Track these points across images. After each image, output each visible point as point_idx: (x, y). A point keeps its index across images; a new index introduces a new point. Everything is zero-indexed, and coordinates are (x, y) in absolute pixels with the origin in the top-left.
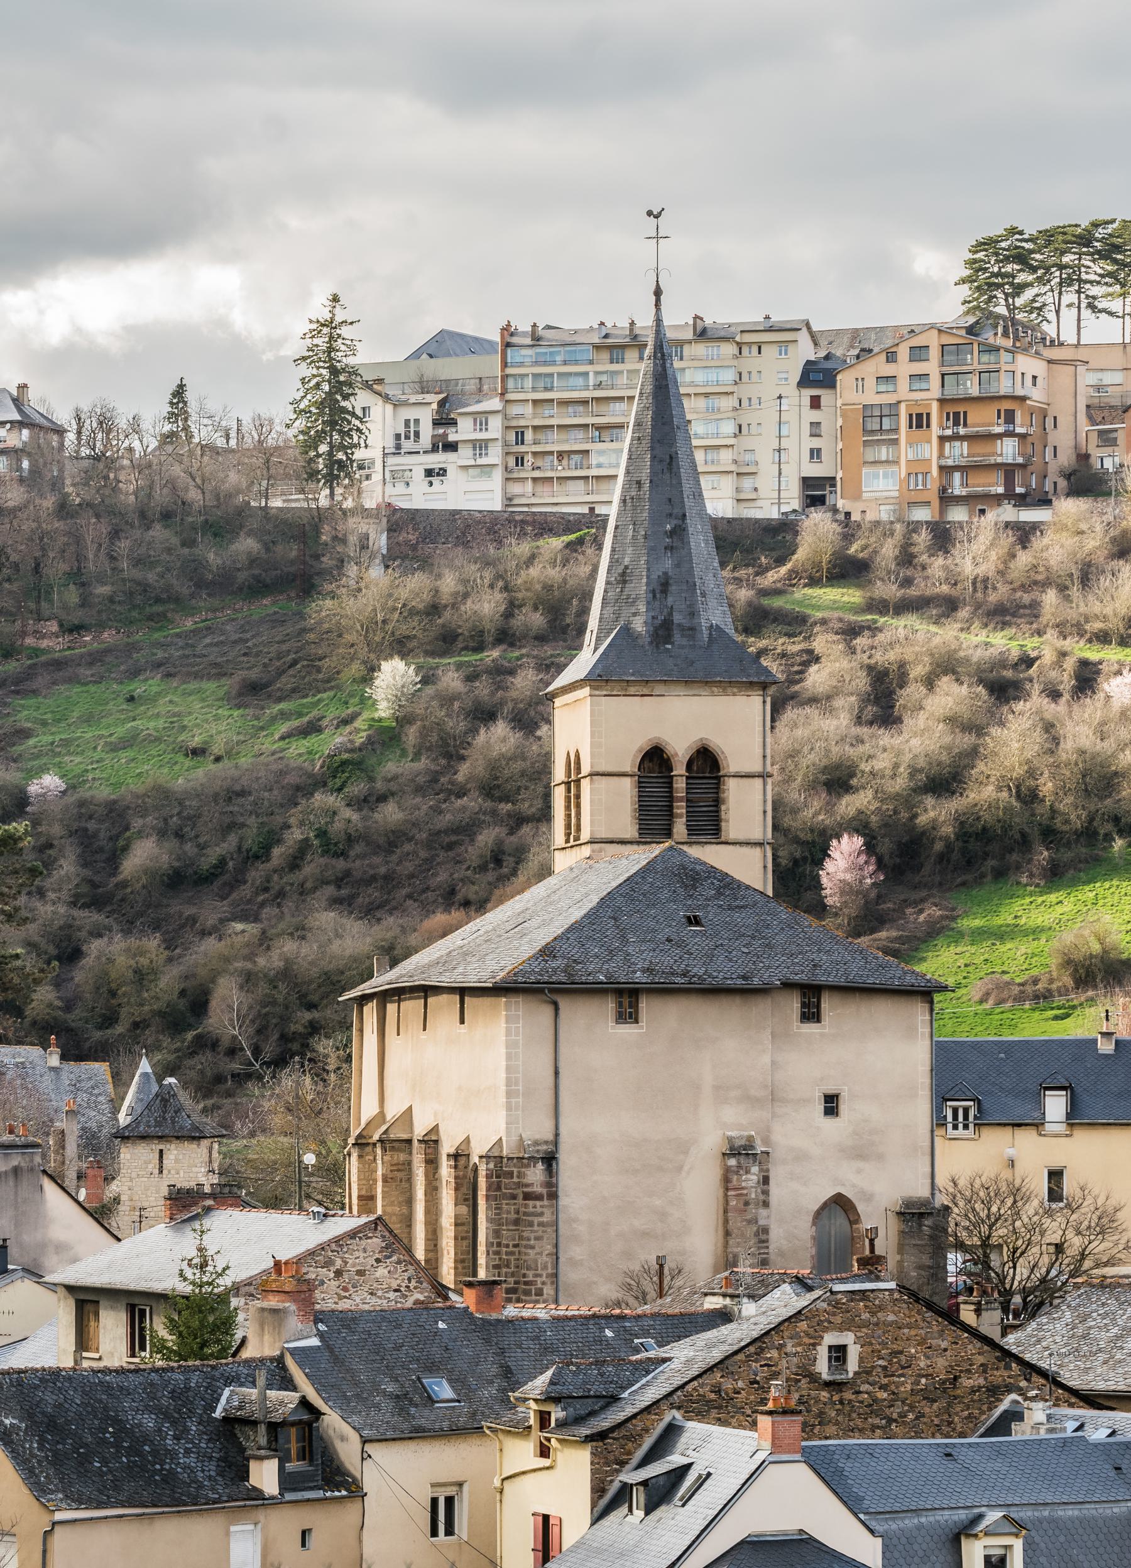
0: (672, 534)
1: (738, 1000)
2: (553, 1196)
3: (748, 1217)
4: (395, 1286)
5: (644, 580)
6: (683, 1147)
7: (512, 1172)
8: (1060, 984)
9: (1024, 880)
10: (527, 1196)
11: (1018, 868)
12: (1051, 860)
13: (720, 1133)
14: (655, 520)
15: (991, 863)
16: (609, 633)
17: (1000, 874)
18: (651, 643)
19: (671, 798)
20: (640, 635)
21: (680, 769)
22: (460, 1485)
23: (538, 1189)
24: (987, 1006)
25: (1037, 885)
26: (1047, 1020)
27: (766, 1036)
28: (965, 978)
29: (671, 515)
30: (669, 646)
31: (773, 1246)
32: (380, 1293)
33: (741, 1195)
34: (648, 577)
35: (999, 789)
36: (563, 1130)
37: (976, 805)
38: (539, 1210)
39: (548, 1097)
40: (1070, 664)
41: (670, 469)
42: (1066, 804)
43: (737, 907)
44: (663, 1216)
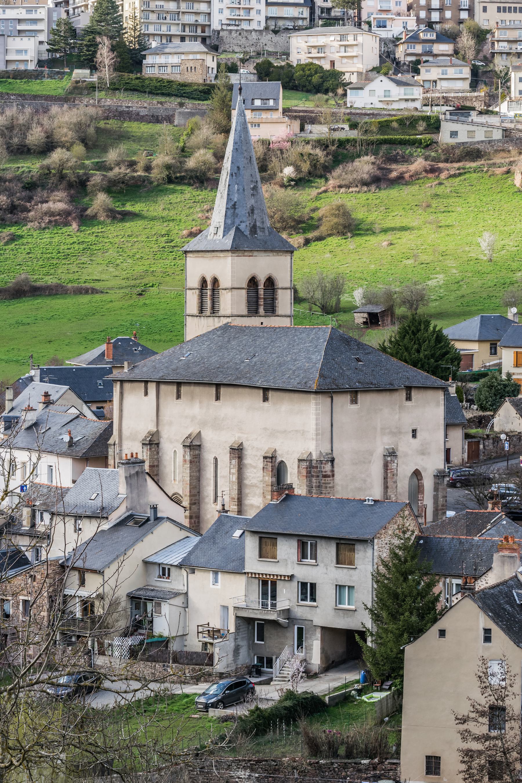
1: (388, 393)
2: (333, 476)
10: (325, 476)
19: (258, 298)
21: (261, 286)
23: (329, 473)
41: (250, 162)
44: (365, 481)
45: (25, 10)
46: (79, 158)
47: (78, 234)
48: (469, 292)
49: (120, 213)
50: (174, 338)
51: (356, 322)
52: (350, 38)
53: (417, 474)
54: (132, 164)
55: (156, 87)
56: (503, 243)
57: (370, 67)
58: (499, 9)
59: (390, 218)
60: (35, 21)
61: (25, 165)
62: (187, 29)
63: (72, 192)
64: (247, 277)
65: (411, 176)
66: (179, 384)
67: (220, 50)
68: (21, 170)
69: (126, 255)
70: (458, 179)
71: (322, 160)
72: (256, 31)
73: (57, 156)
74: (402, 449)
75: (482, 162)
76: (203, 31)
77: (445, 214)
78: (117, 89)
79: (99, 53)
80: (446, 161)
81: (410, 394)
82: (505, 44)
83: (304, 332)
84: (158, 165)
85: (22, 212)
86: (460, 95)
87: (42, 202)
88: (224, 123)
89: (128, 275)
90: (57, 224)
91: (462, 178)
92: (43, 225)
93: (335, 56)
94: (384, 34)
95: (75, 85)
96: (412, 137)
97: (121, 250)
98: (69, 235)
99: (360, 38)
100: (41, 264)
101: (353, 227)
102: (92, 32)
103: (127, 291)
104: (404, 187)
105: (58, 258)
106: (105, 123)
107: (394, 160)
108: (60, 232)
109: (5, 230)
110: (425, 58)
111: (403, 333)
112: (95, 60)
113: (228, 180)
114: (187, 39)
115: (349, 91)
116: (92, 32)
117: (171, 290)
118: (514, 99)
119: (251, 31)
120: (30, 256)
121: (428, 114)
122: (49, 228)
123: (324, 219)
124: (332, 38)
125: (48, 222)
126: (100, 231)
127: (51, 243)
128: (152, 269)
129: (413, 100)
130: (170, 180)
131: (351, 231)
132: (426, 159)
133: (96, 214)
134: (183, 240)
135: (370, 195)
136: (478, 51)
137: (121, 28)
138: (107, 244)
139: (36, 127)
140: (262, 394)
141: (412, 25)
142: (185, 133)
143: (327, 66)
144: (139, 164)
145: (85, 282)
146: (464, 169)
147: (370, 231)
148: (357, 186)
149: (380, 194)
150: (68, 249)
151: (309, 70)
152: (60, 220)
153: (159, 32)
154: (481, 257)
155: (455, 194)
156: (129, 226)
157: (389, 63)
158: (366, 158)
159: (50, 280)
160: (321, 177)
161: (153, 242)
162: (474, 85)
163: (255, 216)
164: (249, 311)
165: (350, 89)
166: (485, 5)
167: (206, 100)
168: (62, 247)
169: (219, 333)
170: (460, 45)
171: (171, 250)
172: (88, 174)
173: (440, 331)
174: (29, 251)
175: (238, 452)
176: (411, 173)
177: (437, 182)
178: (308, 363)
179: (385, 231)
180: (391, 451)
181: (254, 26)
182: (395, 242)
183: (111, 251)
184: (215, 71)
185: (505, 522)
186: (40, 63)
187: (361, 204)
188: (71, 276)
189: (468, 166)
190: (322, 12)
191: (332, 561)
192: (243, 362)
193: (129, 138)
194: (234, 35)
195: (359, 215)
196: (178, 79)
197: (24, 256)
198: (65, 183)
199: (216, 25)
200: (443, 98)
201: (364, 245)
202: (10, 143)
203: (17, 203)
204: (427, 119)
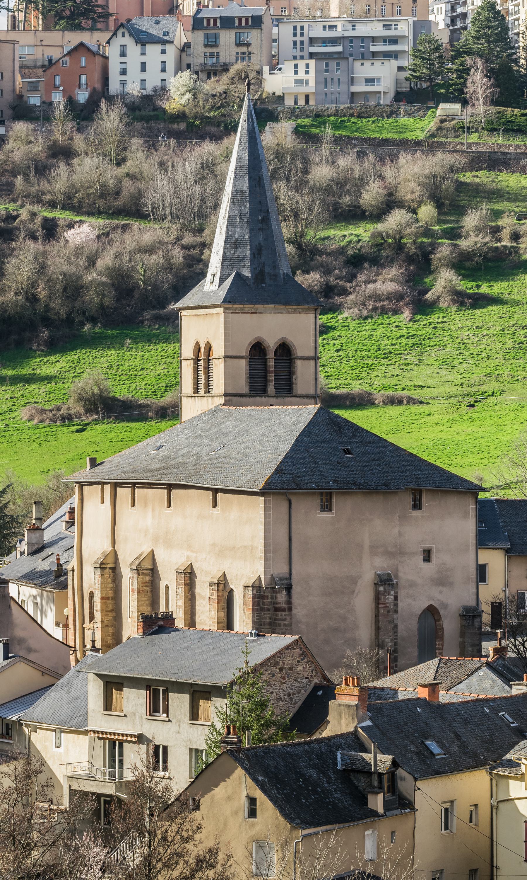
0: (263, 220)
2: (290, 609)
3: (390, 619)
4: (306, 675)
5: (248, 247)
6: (354, 580)
7: (268, 596)
8: (75, 411)
9: (35, 348)
11: (30, 341)
12: (50, 337)
13: (373, 572)
14: (252, 212)
15: (13, 337)
16: (229, 275)
17: (19, 344)
18: (254, 283)
19: (266, 371)
21: (271, 355)
22: (452, 802)
23: (283, 606)
24: (35, 422)
25: (42, 351)
26: (73, 432)
27: (396, 517)
28: (13, 405)
29: (261, 210)
30: (264, 285)
31: (399, 635)
32: (299, 680)
33: (386, 607)
34: (250, 246)
35: (16, 294)
36: (294, 572)
37: (3, 303)
38: (284, 617)
39: (286, 552)
40: (38, 220)
42: (56, 303)
43: (366, 443)
44: (344, 619)
45: (381, 24)
47: (410, 325)
49: (470, 296)
53: (432, 612)
60: (394, 40)
64: (248, 342)
68: (347, 239)
69: (467, 354)
73: (396, 219)
78: (495, 130)
81: (420, 500)
85: (340, 295)
89: (463, 380)
90: (384, 311)
92: (365, 313)
95: (439, 124)
97: (464, 346)
98: (397, 326)
100: (351, 364)
106: (474, 176)
112: (466, 90)
113: (228, 208)
117: (514, 400)
120: (340, 353)
122: (372, 318)
125: (372, 309)
126: (439, 321)
127: (370, 337)
128: (497, 372)
133: (438, 298)
138: (446, 338)
144: (504, 230)
145: (404, 389)
152: (384, 307)
156: (480, 314)
159: (357, 387)
161: (508, 336)
163: (263, 259)
164: (252, 388)
168: (384, 343)
172: (435, 243)
174: (339, 347)
175: (189, 577)
180: (384, 578)
183: (448, 348)
191: (185, 715)
193: (502, 196)
197: (332, 353)
198: (403, 256)
202: (339, 203)
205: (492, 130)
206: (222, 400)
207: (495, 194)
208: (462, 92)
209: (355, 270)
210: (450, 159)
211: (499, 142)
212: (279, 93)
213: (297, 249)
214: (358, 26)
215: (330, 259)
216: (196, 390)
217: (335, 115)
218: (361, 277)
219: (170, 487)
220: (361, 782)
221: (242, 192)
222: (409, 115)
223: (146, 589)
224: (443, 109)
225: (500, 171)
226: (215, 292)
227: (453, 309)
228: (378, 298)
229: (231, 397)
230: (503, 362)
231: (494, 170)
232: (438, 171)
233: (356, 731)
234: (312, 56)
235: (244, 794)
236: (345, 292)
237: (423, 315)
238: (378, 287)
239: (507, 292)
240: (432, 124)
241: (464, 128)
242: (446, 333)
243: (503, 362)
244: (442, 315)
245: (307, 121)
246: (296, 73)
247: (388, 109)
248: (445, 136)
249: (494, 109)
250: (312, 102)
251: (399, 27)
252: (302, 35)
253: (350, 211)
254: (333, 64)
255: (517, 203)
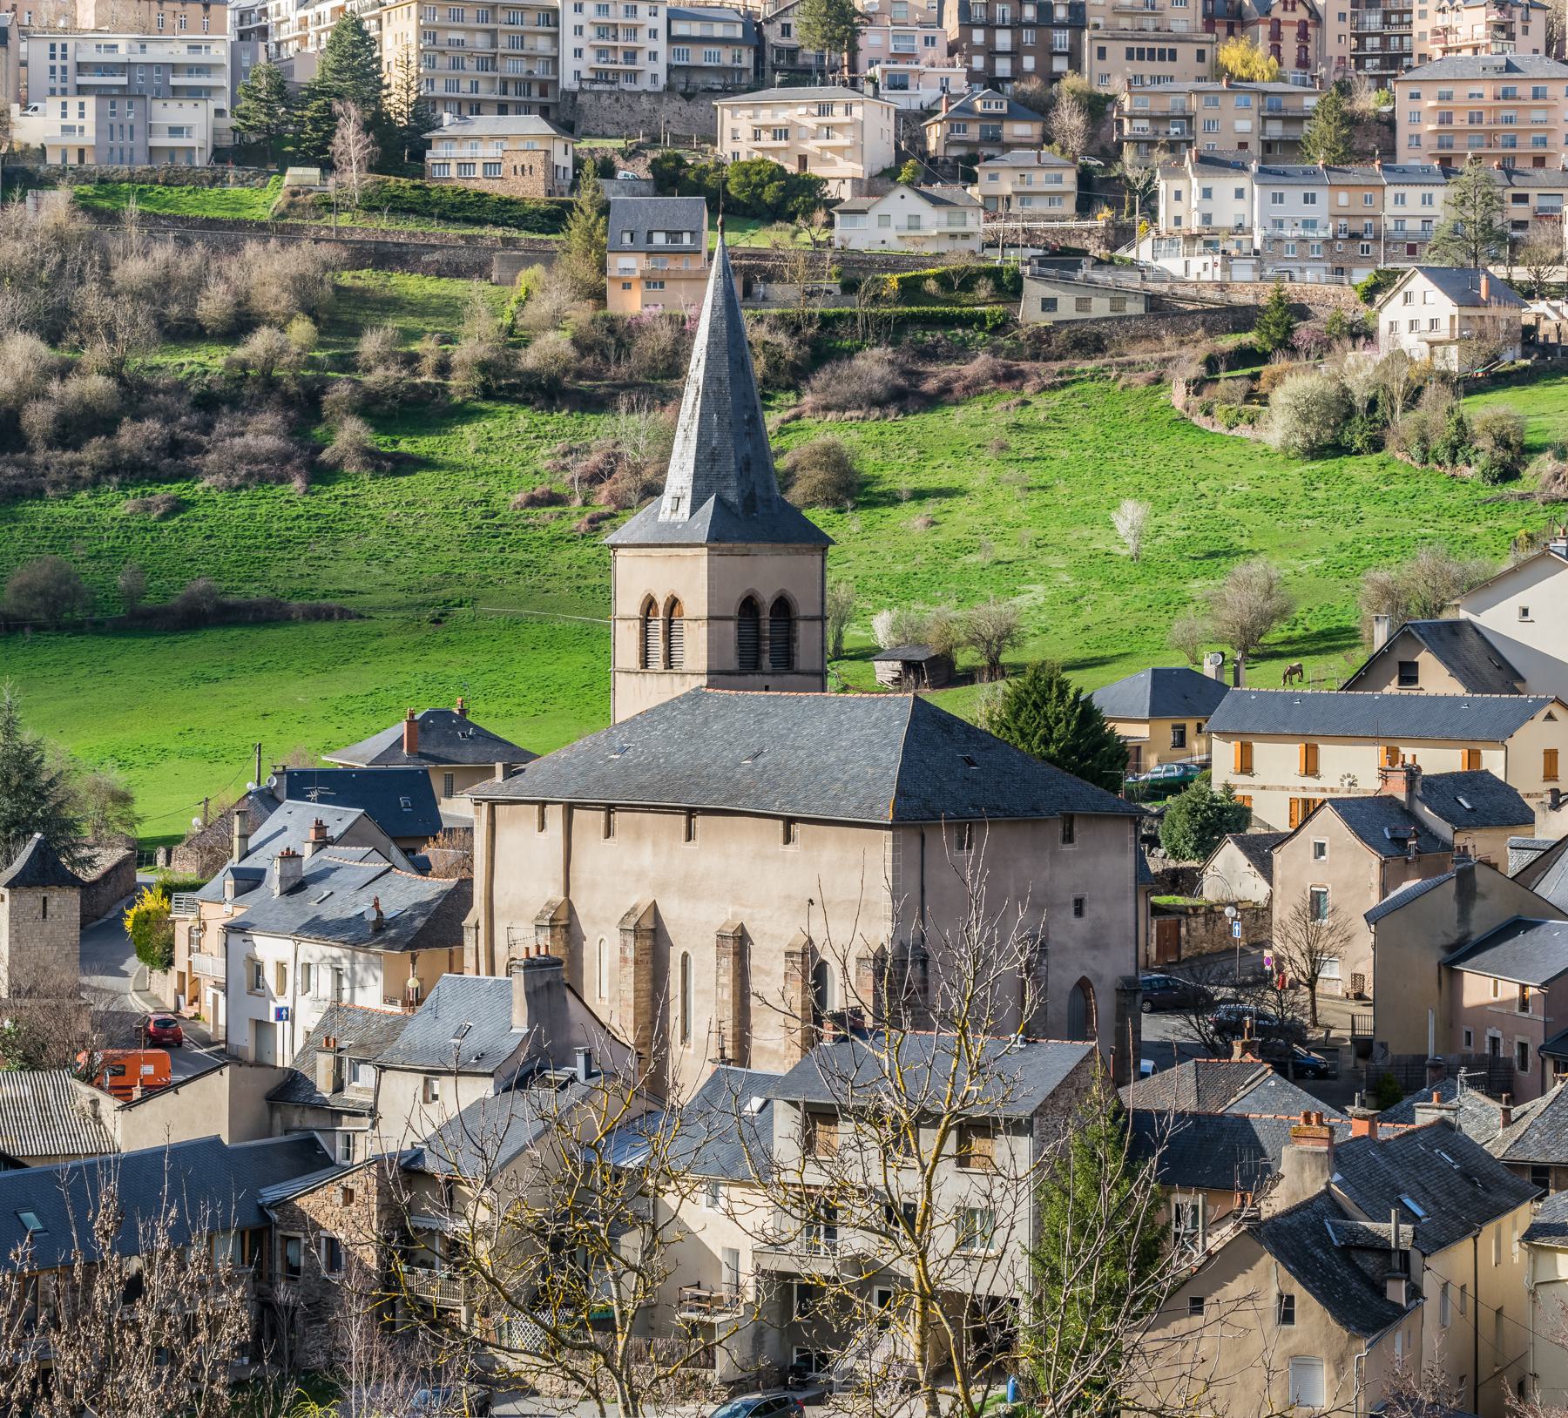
19: (758, 637)
20: (733, 504)
21: (766, 615)
45: (185, 46)
46: (303, 347)
47: (307, 499)
48: (1098, 620)
49: (388, 457)
50: (515, 710)
51: (878, 679)
52: (839, 111)
53: (1084, 985)
54: (411, 360)
55: (453, 205)
56: (1157, 521)
57: (877, 169)
58: (1130, 54)
59: (927, 471)
61: (196, 359)
62: (511, 89)
63: (291, 414)
65: (966, 388)
66: (610, 809)
67: (577, 132)
68: (187, 369)
70: (1059, 395)
71: (790, 355)
72: (649, 94)
73: (260, 342)
74: (1058, 937)
75: (1106, 360)
76: (543, 93)
77: (1036, 463)
78: (376, 209)
79: (339, 135)
80: (1035, 357)
82: (1145, 124)
83: (859, 706)
84: (463, 363)
85: (193, 453)
86: (1057, 225)
87: (233, 435)
88: (592, 277)
90: (263, 479)
91: (1067, 391)
92: (236, 481)
93: (811, 146)
94: (902, 100)
96: (966, 310)
98: (288, 501)
99: (858, 112)
101: (855, 489)
102: (323, 93)
103: (409, 614)
104: (953, 410)
105: (268, 548)
106: (354, 277)
107: (929, 354)
108: (271, 494)
109: (158, 491)
110: (986, 151)
111: (1018, 704)
113: (699, 403)
114: (511, 108)
115: (837, 217)
116: (323, 93)
118: (1164, 233)
119: (638, 94)
120: (212, 542)
121: (997, 264)
122: (247, 488)
123: (799, 474)
124: (802, 110)
126: (350, 492)
127: (252, 517)
128: (457, 571)
129: (966, 236)
130: (487, 393)
131: (850, 496)
132: (996, 351)
133: (341, 459)
134: (517, 513)
135: (886, 425)
136: (1091, 137)
137: (380, 85)
138: (366, 520)
139: (216, 285)
140: (781, 830)
141: (959, 82)
142: (514, 298)
143: (792, 168)
145: (325, 596)
146: (1071, 373)
147: (893, 499)
148: (860, 407)
149: (906, 424)
150: (288, 529)
151: (759, 173)
152: (263, 472)
153: (455, 95)
154: (1116, 549)
155: (1053, 424)
157: (916, 165)
158: (877, 351)
159: (255, 592)
160: (788, 388)
162: (1085, 207)
165: (841, 212)
166: (1102, 44)
167: (556, 232)
169: (684, 707)
170: (1055, 125)
171: (493, 532)
173: (1089, 699)
175: (739, 944)
176: (966, 382)
177: (1018, 398)
178: (872, 766)
179: (919, 495)
181: (644, 84)
182: (940, 518)
183: (373, 535)
184: (570, 175)
185: (1273, 1083)
186: (219, 155)
187: (866, 440)
188: (295, 584)
189: (1078, 368)
190: (779, 57)
192: (739, 765)
193: (402, 308)
194: (605, 101)
195: (868, 462)
196: (497, 190)
199: (568, 82)
200: (1024, 230)
201: (878, 526)
202: (163, 314)
203: (183, 435)
204: (995, 273)
205: (372, 209)
206: (704, 681)
207: (394, 305)
208: (322, 150)
209: (209, 417)
210: (325, 251)
211: (384, 227)
212: (35, 145)
213: (120, 384)
214: (150, 47)
215: (169, 400)
216: (645, 663)
217: (128, 181)
218: (221, 427)
219: (691, 813)
220: (1370, 1264)
221: (719, 379)
222: (242, 184)
223: (646, 958)
224: (297, 175)
225: (391, 270)
226: (684, 524)
227: (366, 476)
228: (254, 460)
229: (717, 675)
230: (460, 555)
231: (383, 269)
232: (309, 268)
233: (1328, 1191)
234: (81, 90)
235: (1275, 1291)
236: (199, 449)
237: (323, 483)
238: (252, 443)
239: (440, 451)
240: (280, 198)
241: (328, 204)
242: (363, 513)
243: (460, 555)
244: (350, 485)
245: (88, 189)
246: (64, 115)
247: (209, 174)
248: (301, 217)
249: (371, 178)
250: (89, 160)
251: (213, 51)
252: (64, 57)
253: (180, 326)
254: (122, 105)
255: (427, 319)
